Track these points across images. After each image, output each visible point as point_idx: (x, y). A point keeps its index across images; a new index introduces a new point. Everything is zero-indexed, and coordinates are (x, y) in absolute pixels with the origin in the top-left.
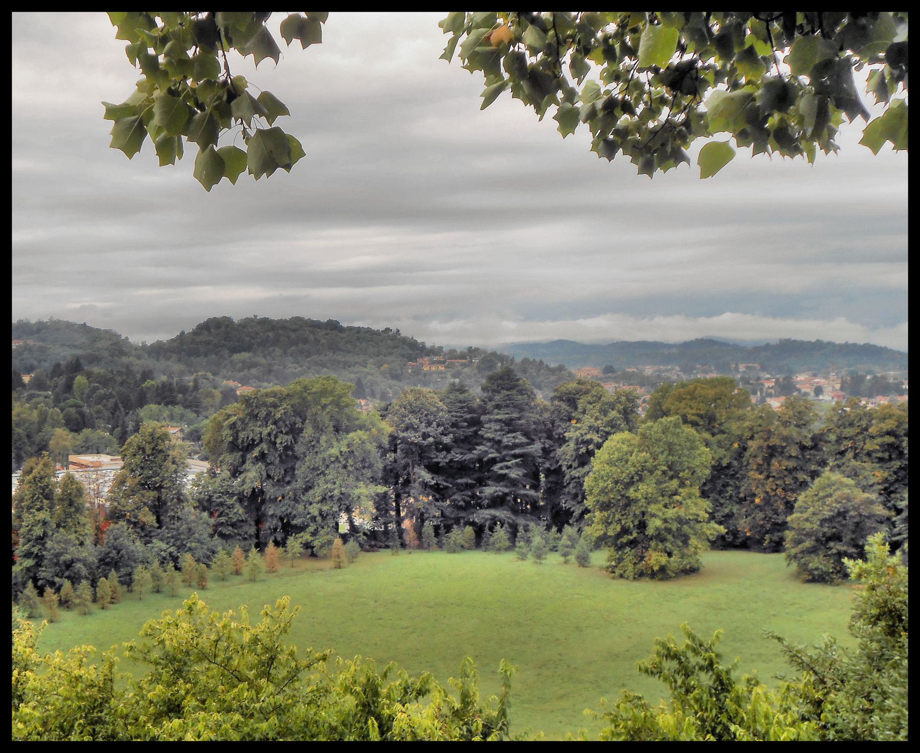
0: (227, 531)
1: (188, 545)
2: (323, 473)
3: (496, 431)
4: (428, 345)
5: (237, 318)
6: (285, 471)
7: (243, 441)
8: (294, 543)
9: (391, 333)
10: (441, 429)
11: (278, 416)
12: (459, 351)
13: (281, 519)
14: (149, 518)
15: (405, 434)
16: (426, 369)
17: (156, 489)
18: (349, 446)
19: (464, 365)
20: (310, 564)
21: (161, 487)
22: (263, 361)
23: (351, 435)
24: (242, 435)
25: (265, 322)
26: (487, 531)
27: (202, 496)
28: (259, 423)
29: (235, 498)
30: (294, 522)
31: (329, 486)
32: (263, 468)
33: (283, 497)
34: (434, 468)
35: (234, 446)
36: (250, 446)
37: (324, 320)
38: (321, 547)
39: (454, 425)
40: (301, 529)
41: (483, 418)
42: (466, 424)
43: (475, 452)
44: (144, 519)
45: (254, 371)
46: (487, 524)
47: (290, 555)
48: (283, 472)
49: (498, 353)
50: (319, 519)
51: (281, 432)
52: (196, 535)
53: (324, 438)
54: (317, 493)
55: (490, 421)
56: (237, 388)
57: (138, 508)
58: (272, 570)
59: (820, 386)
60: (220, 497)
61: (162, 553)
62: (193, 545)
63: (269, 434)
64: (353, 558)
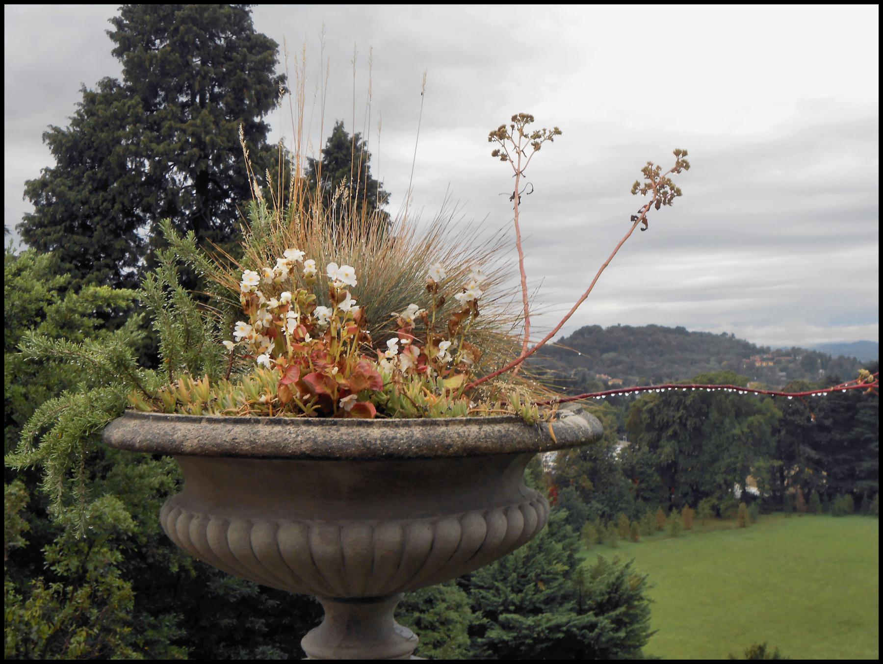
0: (647, 494)
1: (620, 505)
2: (727, 449)
3: (871, 415)
4: (758, 345)
5: (604, 326)
6: (694, 447)
7: (659, 423)
8: (704, 505)
9: (727, 337)
10: (822, 414)
11: (688, 402)
12: (784, 351)
13: (691, 486)
14: (587, 484)
15: (792, 418)
16: (758, 364)
17: (591, 460)
18: (749, 427)
19: (790, 362)
20: (717, 523)
21: (596, 459)
22: (627, 359)
23: (750, 419)
24: (658, 418)
25: (627, 329)
26: (865, 499)
27: (626, 466)
28: (672, 408)
29: (654, 468)
30: (703, 488)
31: (733, 459)
32: (676, 444)
33: (692, 468)
34: (815, 446)
35: (650, 427)
36: (664, 427)
37: (673, 326)
38: (727, 509)
39: (833, 410)
40: (707, 494)
41: (858, 405)
42: (842, 410)
43: (853, 433)
44: (584, 484)
45: (620, 367)
46: (866, 493)
47: (701, 516)
48: (692, 448)
49: (817, 352)
50: (724, 486)
51: (691, 416)
52: (626, 498)
53: (727, 420)
54: (722, 464)
55: (865, 407)
56: (608, 380)
57: (579, 476)
58: (688, 528)
59: (11, 484)
60: (641, 467)
61: (599, 512)
62: (624, 505)
63: (680, 418)
64: (754, 519)
